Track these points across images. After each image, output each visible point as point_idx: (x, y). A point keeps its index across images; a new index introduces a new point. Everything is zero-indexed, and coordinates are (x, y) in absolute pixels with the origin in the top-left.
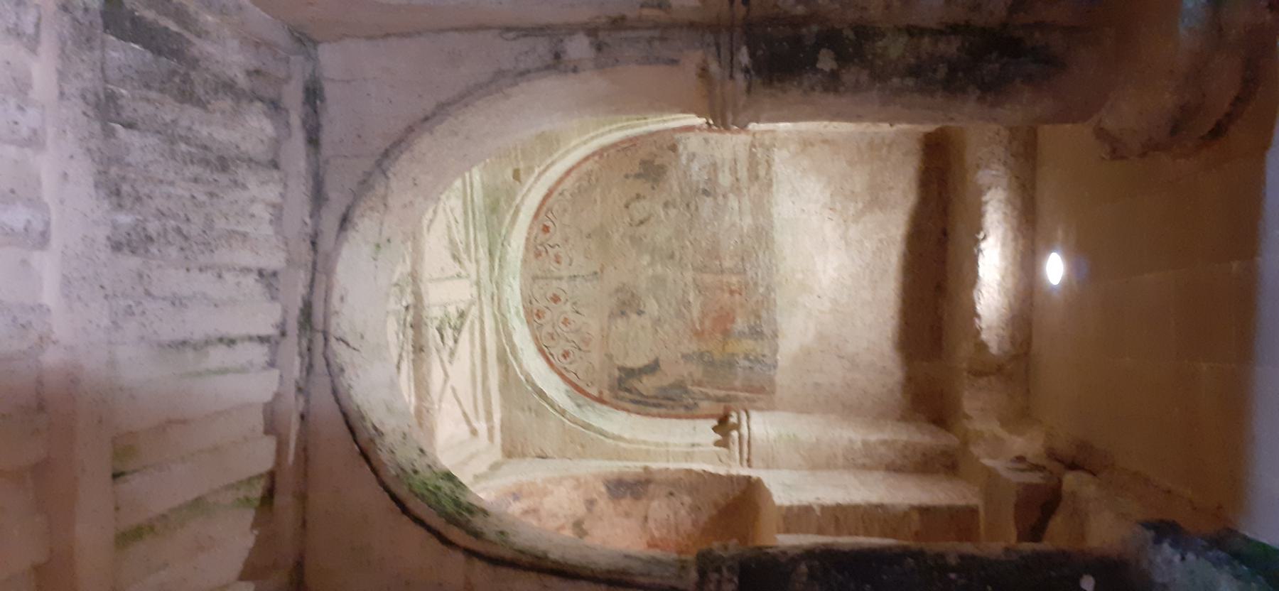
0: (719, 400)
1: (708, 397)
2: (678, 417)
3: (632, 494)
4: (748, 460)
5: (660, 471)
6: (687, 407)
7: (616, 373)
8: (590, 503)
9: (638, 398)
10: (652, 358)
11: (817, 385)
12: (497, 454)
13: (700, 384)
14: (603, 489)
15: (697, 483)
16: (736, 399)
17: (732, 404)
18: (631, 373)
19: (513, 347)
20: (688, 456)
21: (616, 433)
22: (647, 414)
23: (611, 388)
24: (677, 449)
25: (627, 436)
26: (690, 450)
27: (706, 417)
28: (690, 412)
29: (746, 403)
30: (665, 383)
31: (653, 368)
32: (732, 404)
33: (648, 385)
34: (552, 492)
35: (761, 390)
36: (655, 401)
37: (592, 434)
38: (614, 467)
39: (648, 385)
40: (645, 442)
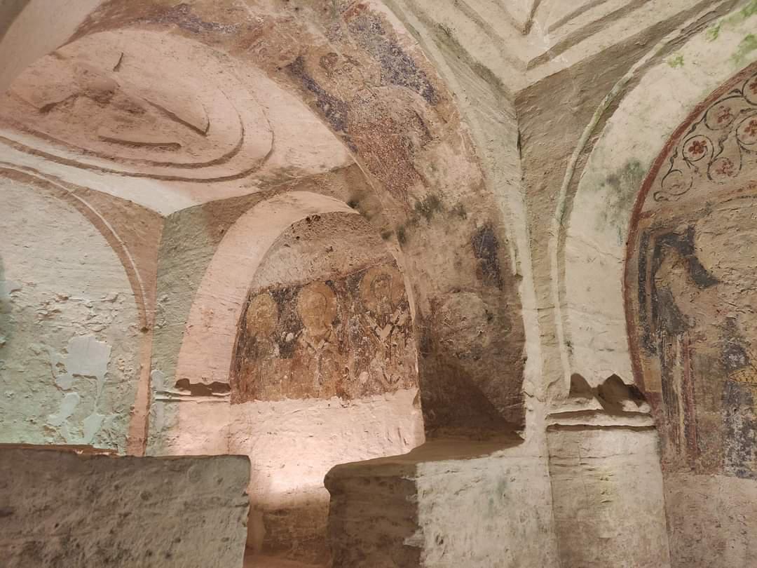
0: (666, 383)
1: (667, 367)
2: (630, 329)
3: (483, 265)
4: (557, 427)
5: (516, 297)
6: (646, 338)
7: (682, 227)
8: (461, 212)
9: (649, 268)
10: (717, 274)
11: (721, 547)
12: (516, 81)
13: (687, 353)
14: (480, 224)
15: (509, 353)
16: (673, 411)
17: (662, 406)
18: (686, 248)
19: (681, 41)
20: (550, 339)
21: (570, 231)
22: (627, 286)
23: (659, 227)
24: (558, 322)
25: (569, 247)
26: (561, 339)
27: (637, 369)
28: (639, 345)
29: (668, 427)
30: (679, 301)
31: (702, 279)
32: (662, 406)
33: (674, 277)
34: (457, 153)
35: (694, 451)
36: (648, 291)
37: (561, 198)
38: (516, 232)
39: (674, 277)
40: (562, 274)
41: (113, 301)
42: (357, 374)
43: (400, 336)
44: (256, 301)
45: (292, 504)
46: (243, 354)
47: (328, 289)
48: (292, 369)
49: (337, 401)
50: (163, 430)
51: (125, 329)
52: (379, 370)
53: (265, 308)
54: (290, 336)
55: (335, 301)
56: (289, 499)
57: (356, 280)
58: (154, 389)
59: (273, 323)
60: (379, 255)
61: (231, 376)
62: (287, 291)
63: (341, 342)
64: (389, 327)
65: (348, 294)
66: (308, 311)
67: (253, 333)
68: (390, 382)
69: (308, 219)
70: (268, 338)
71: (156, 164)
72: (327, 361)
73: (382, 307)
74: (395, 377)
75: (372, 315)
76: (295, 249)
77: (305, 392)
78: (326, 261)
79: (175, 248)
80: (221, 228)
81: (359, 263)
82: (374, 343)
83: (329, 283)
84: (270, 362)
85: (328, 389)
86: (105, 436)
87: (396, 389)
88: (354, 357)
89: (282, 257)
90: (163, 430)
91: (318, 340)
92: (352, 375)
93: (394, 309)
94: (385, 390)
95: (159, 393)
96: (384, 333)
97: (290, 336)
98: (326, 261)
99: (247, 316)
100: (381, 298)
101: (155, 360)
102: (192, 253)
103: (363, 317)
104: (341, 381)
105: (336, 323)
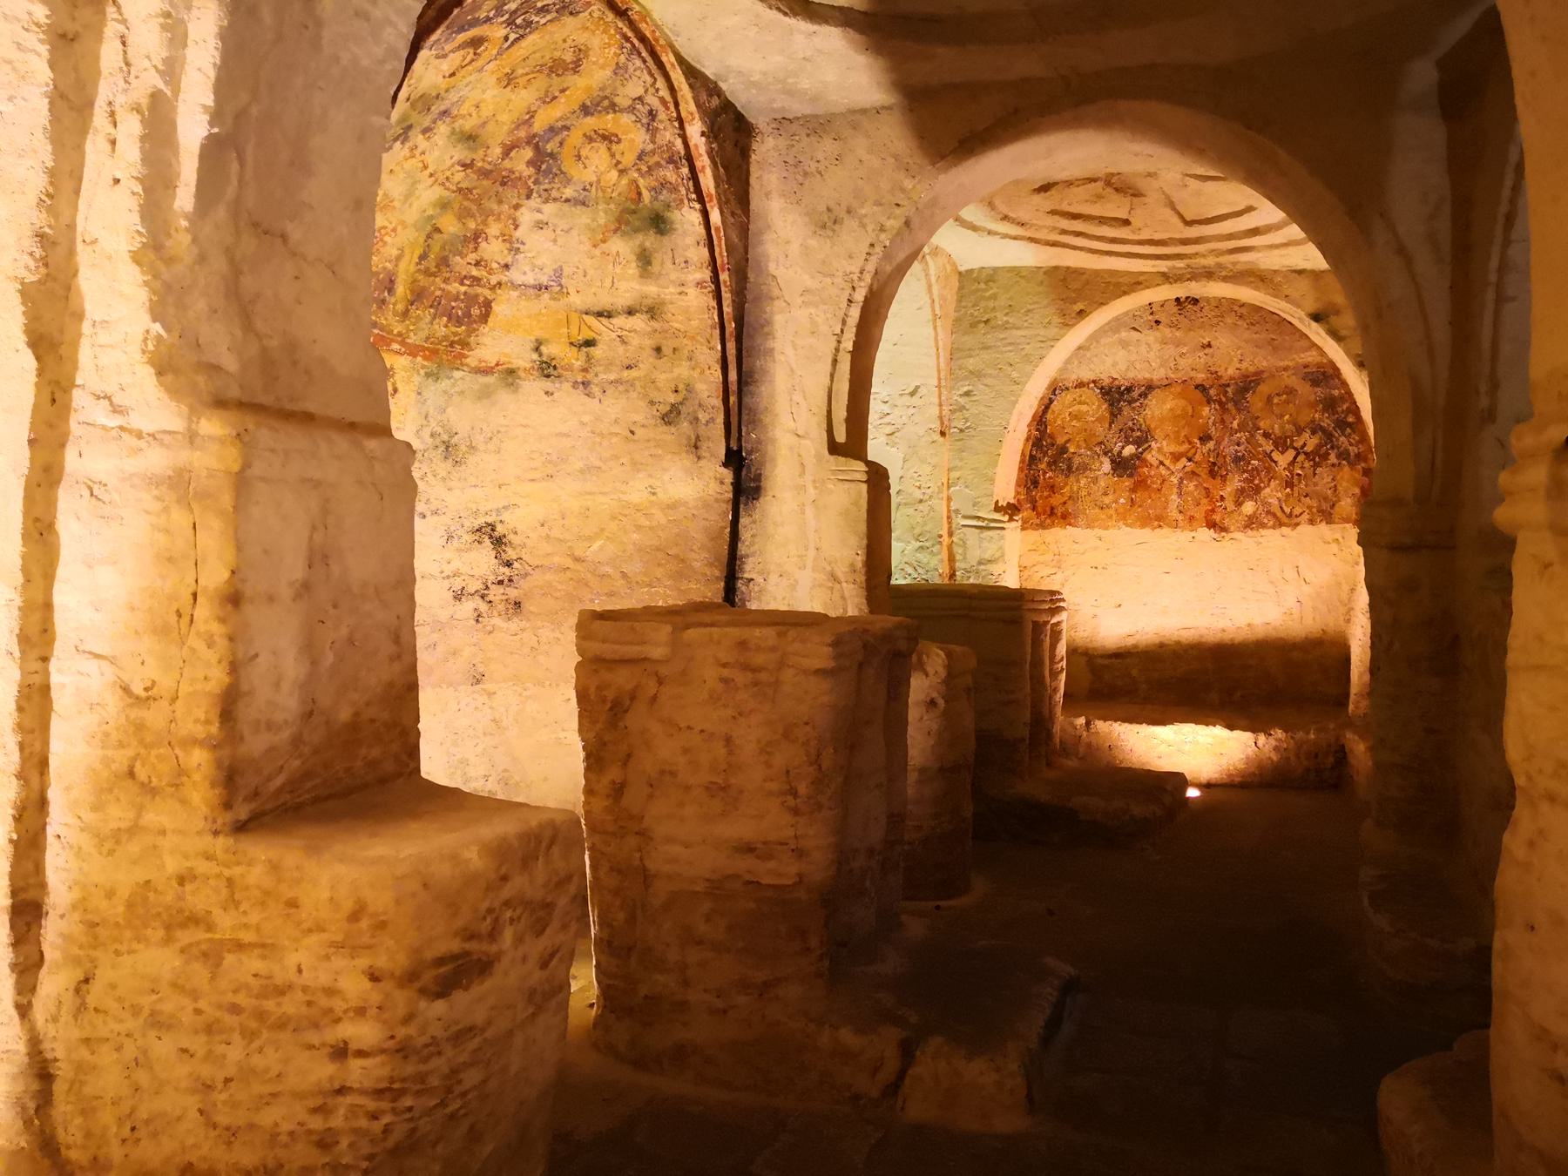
41: (912, 394)
42: (1239, 504)
43: (1307, 464)
44: (1068, 397)
45: (1135, 646)
46: (1043, 466)
47: (1198, 395)
48: (1133, 490)
49: (1205, 534)
50: (980, 563)
51: (921, 432)
52: (1274, 501)
53: (1084, 408)
54: (1129, 450)
55: (1206, 411)
56: (1130, 642)
57: (1245, 390)
58: (957, 511)
59: (1100, 430)
60: (1286, 363)
61: (1018, 493)
62: (1129, 390)
63: (1214, 464)
64: (1291, 454)
65: (1230, 406)
66: (1162, 420)
67: (1060, 440)
68: (1290, 516)
69: (1178, 299)
70: (1090, 449)
71: (1064, 232)
72: (1190, 486)
73: (1282, 427)
74: (1297, 511)
75: (1266, 435)
76: (1150, 337)
77: (1157, 520)
78: (1201, 359)
79: (986, 322)
80: (1080, 306)
81: (1252, 369)
82: (1268, 469)
83: (1201, 388)
84: (1095, 480)
85: (1192, 518)
86: (910, 570)
87: (1297, 524)
88: (1235, 482)
89: (1124, 344)
90: (980, 563)
91: (1176, 457)
92: (1230, 506)
93: (1300, 431)
94: (1281, 525)
95: (965, 517)
96: (1283, 460)
97: (1129, 450)
98: (1201, 359)
99: (1049, 416)
100: (1282, 416)
101: (954, 475)
102: (1020, 333)
103: (1252, 436)
104: (1213, 511)
105: (1205, 439)
